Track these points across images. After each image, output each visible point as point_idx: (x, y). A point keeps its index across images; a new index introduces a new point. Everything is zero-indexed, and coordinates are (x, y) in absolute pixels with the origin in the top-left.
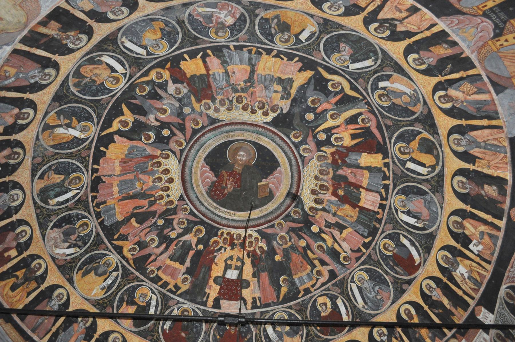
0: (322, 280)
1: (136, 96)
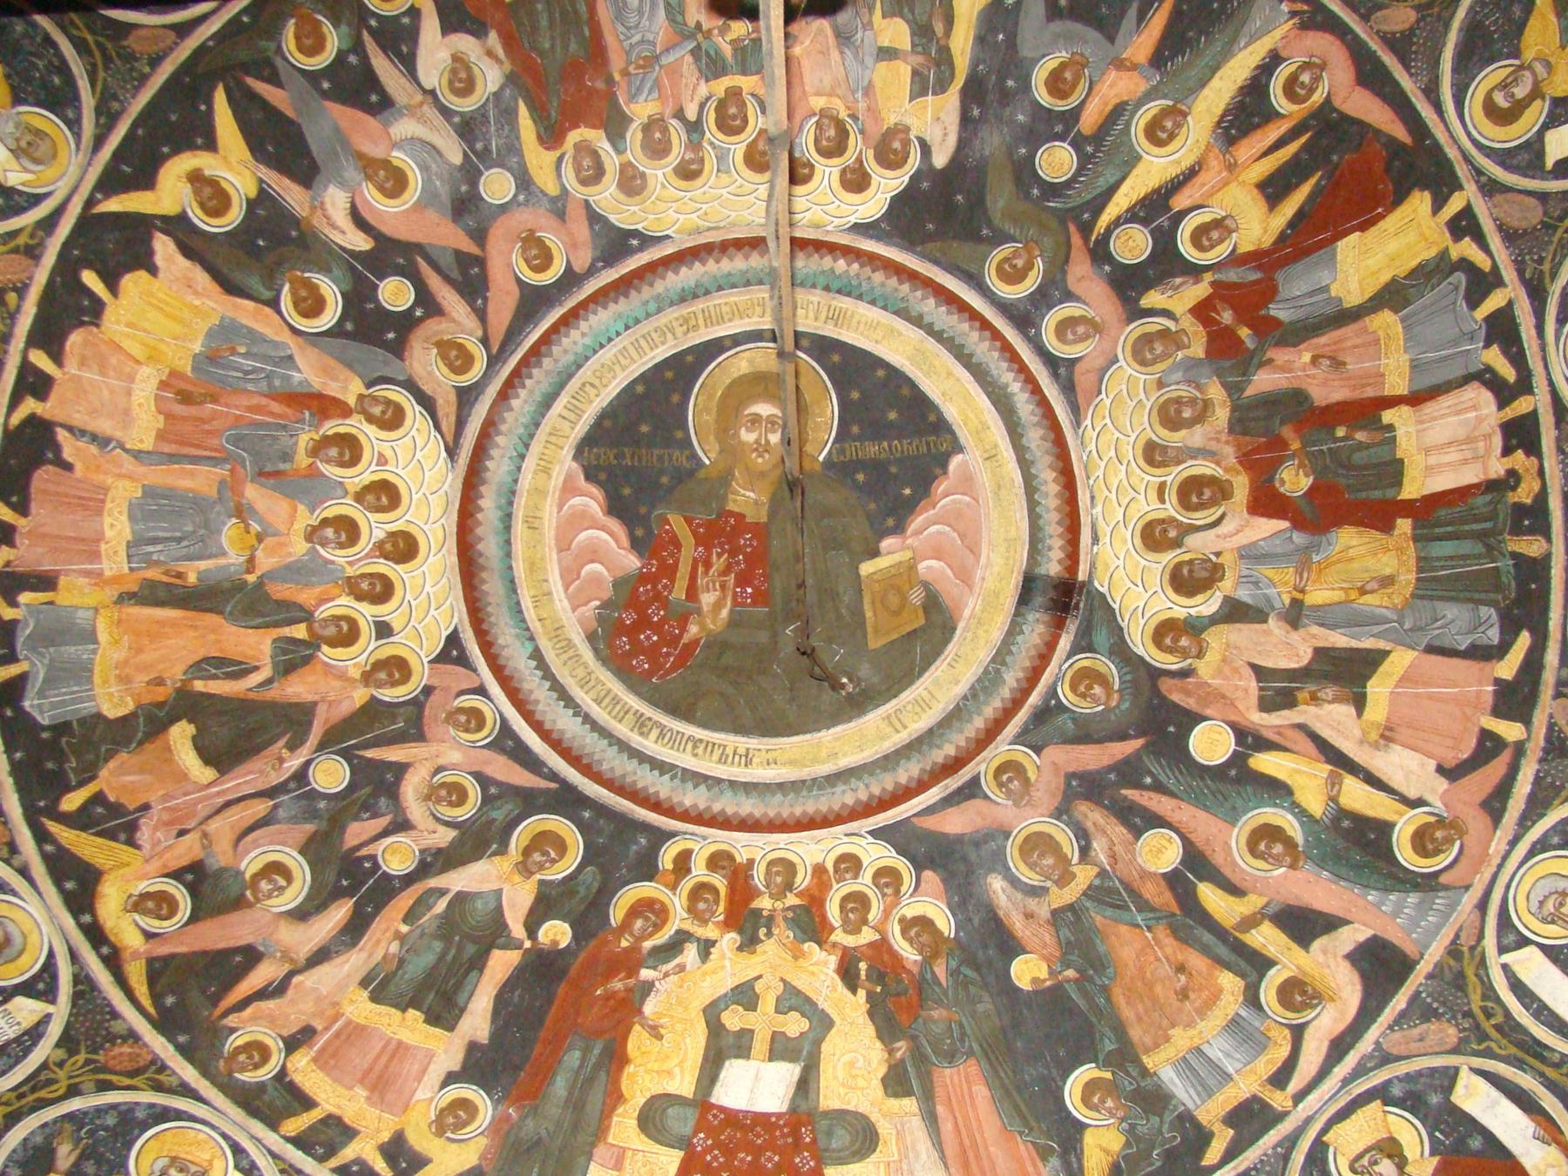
0: (1325, 1024)
1: (279, 62)
